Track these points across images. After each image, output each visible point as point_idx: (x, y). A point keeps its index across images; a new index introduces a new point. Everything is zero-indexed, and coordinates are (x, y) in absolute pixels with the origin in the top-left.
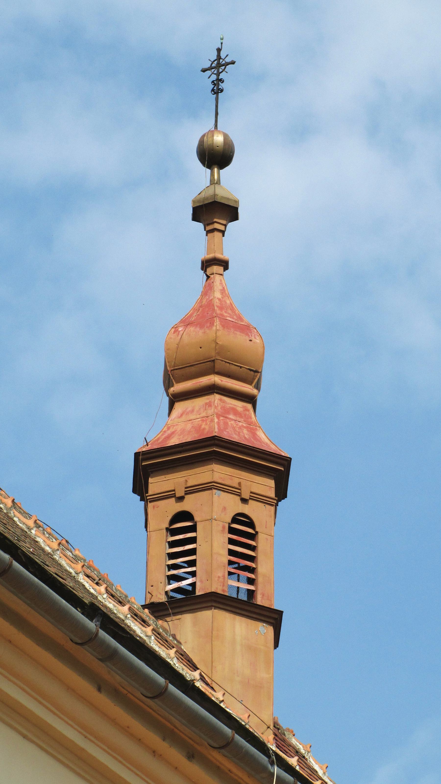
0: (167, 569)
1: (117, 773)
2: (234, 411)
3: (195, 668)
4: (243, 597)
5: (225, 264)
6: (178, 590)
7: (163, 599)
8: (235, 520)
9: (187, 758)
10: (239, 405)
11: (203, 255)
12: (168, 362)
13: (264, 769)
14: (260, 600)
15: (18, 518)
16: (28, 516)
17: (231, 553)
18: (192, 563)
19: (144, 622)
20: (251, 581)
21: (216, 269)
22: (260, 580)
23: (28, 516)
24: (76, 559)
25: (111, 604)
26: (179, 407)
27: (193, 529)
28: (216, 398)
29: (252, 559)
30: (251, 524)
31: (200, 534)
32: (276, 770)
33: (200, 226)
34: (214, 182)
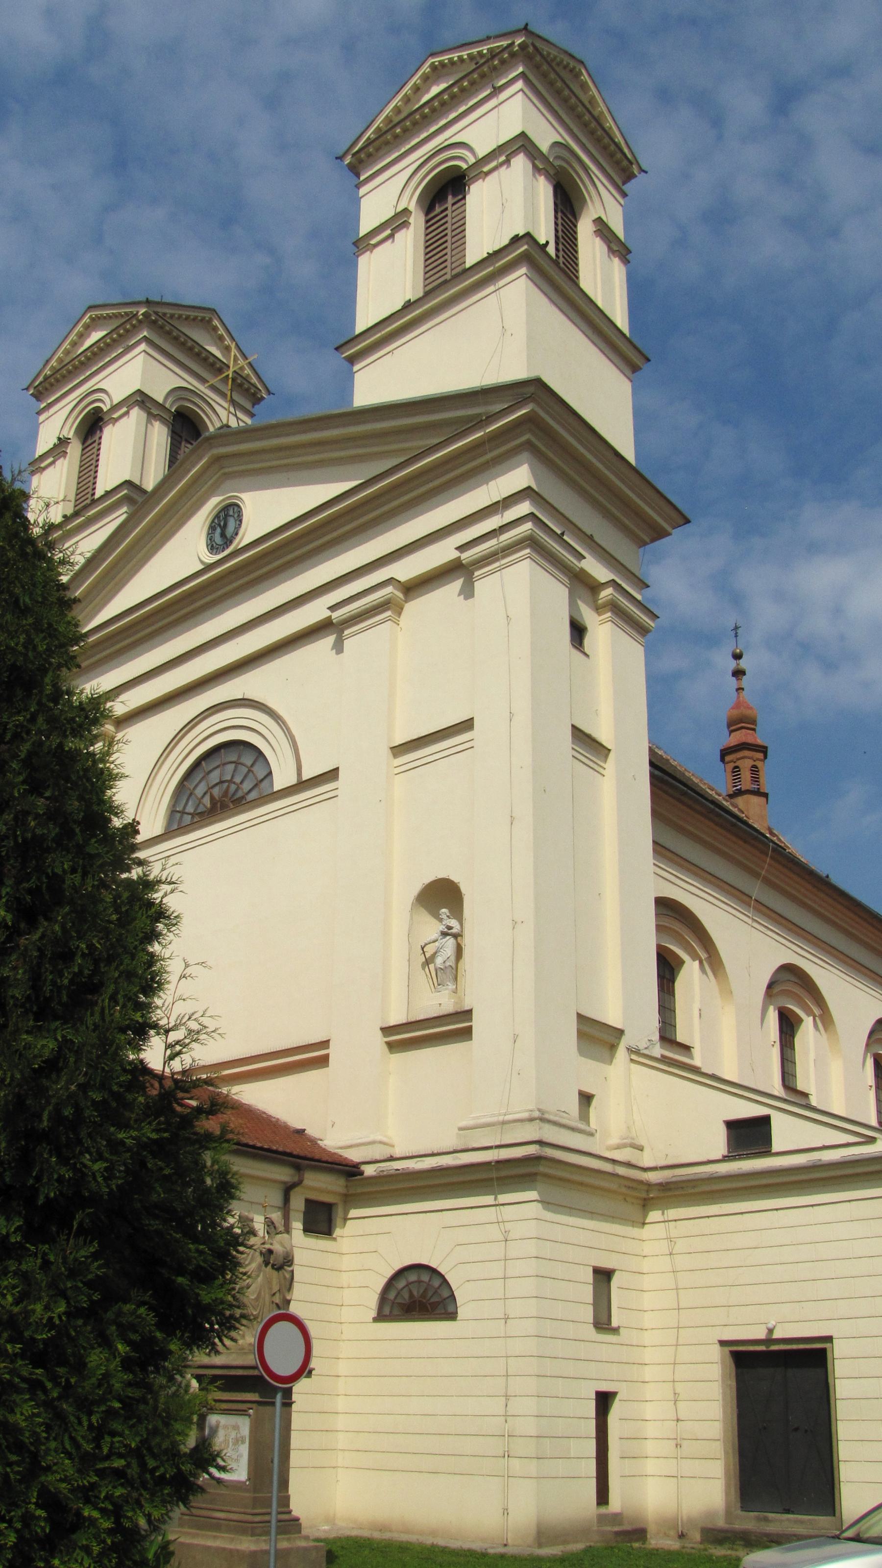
0: (359, 1177)
1: (244, 1102)
2: (749, 734)
3: (743, 813)
4: (756, 790)
5: (743, 689)
6: (737, 790)
7: (732, 793)
8: (752, 767)
9: (220, 1101)
10: (751, 732)
11: (736, 687)
12: (254, 1507)
13: (767, 844)
14: (762, 791)
15: (687, 774)
16: (690, 772)
17: (752, 777)
18: (740, 781)
19: (727, 801)
20: (758, 785)
21: (741, 691)
22: (761, 784)
23: (690, 772)
24: (705, 784)
25: (717, 797)
26: (733, 734)
27: (739, 771)
28: (744, 730)
29: (758, 778)
30: (757, 768)
31: (742, 772)
32: (771, 844)
33: (734, 678)
34: (738, 664)
